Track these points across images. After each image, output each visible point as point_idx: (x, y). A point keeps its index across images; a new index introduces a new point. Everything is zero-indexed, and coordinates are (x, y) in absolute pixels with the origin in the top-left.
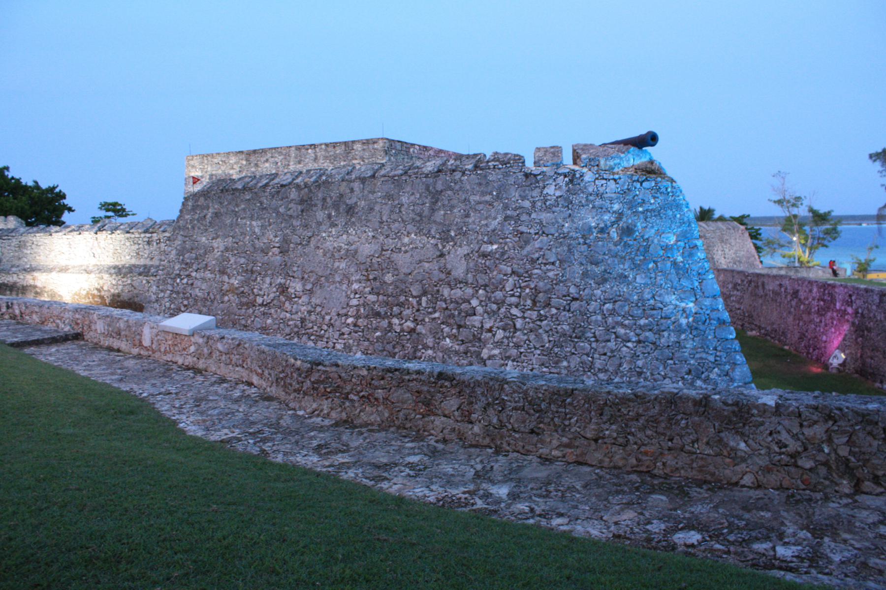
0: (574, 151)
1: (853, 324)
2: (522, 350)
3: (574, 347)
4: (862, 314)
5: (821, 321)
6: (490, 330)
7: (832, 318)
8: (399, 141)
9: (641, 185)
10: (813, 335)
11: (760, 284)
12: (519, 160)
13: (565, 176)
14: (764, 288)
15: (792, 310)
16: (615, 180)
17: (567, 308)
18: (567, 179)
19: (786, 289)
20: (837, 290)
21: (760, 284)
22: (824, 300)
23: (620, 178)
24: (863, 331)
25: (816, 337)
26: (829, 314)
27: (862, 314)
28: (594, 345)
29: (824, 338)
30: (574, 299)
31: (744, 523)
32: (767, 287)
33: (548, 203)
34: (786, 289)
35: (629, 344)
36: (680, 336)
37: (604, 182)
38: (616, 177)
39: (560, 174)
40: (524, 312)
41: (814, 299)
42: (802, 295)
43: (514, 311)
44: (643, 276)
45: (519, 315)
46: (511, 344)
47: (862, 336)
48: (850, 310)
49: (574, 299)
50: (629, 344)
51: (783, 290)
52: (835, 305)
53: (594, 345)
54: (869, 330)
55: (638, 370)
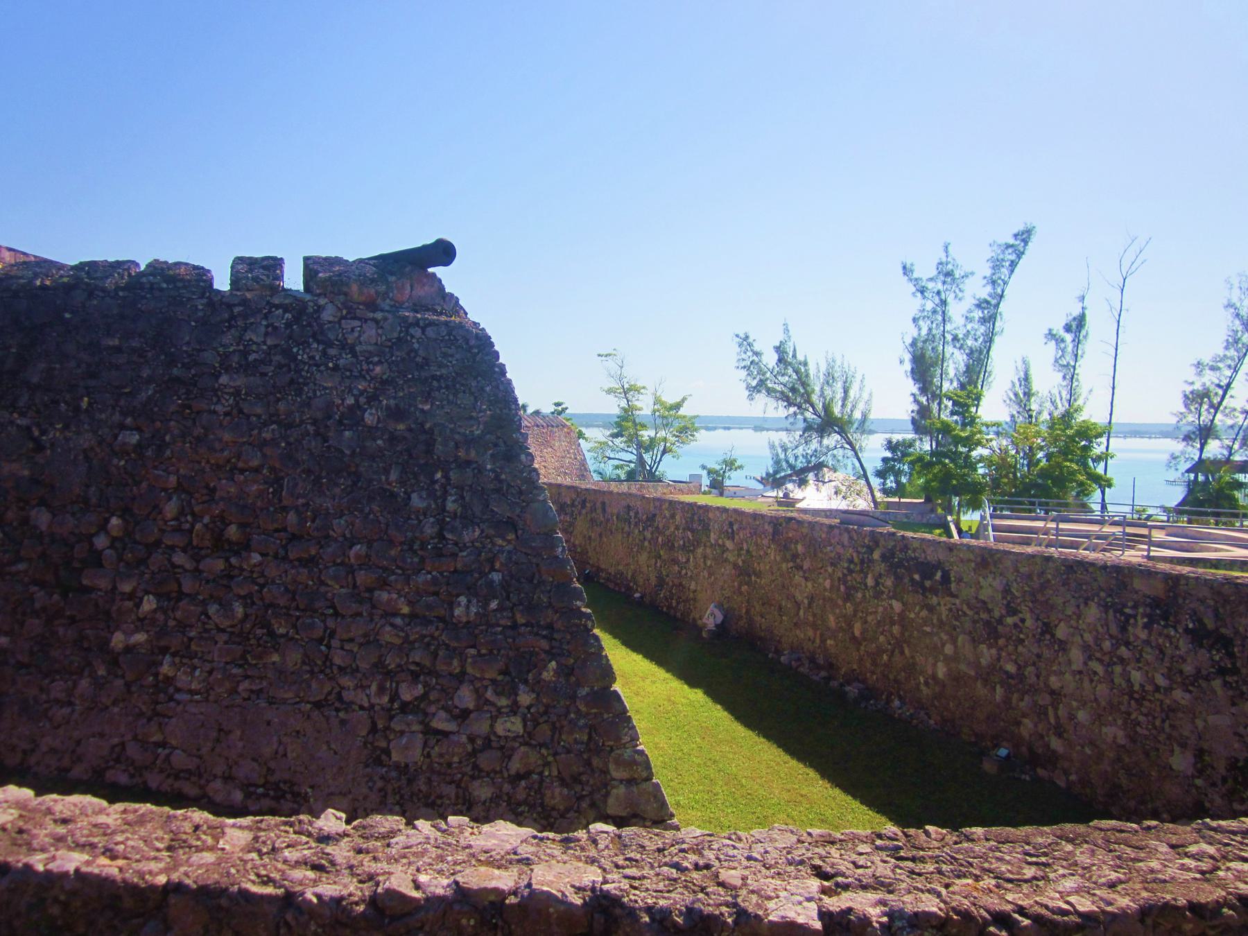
0: (306, 267)
1: (735, 566)
2: (193, 634)
3: (294, 626)
4: (748, 551)
5: (688, 560)
6: (131, 596)
7: (705, 557)
8: (10, 250)
9: (423, 332)
10: (676, 581)
11: (599, 505)
12: (202, 277)
13: (286, 311)
14: (604, 510)
15: (646, 543)
16: (376, 321)
17: (282, 552)
18: (288, 316)
19: (637, 513)
20: (711, 515)
21: (599, 505)
22: (692, 531)
23: (385, 319)
24: (749, 576)
25: (681, 584)
26: (700, 550)
27: (748, 551)
28: (331, 623)
29: (693, 587)
30: (294, 537)
31: (596, 916)
32: (609, 510)
33: (252, 358)
34: (637, 513)
35: (398, 621)
36: (488, 604)
37: (357, 323)
38: (379, 315)
39: (277, 307)
40: (198, 562)
41: (677, 528)
42: (660, 523)
43: (179, 558)
44: (424, 494)
45: (188, 566)
46: (172, 623)
47: (748, 584)
48: (729, 544)
49: (294, 537)
50: (398, 621)
51: (632, 514)
52: (709, 537)
53: (331, 623)
54: (759, 575)
55: (413, 668)
